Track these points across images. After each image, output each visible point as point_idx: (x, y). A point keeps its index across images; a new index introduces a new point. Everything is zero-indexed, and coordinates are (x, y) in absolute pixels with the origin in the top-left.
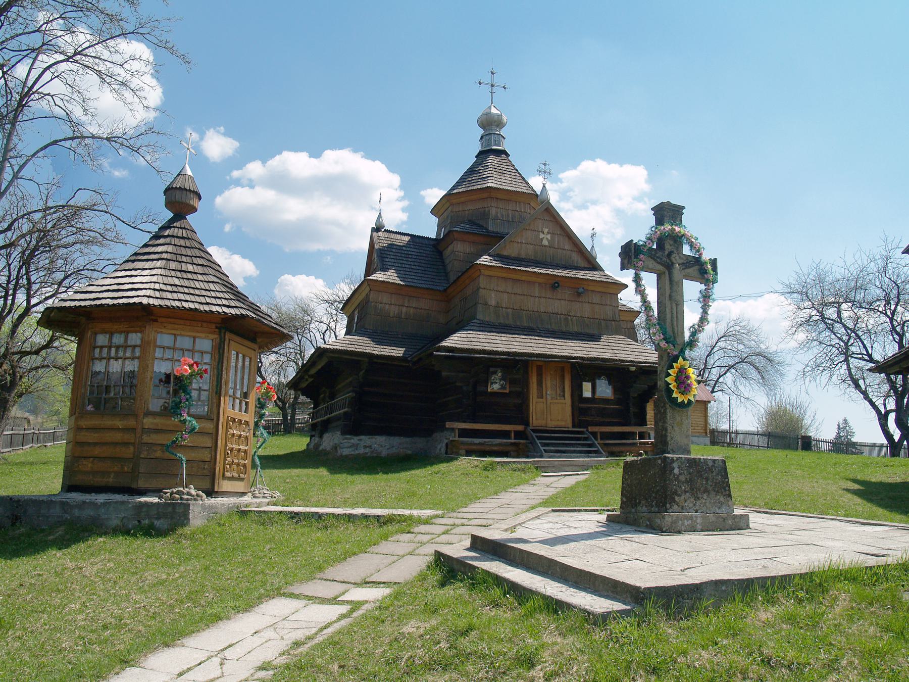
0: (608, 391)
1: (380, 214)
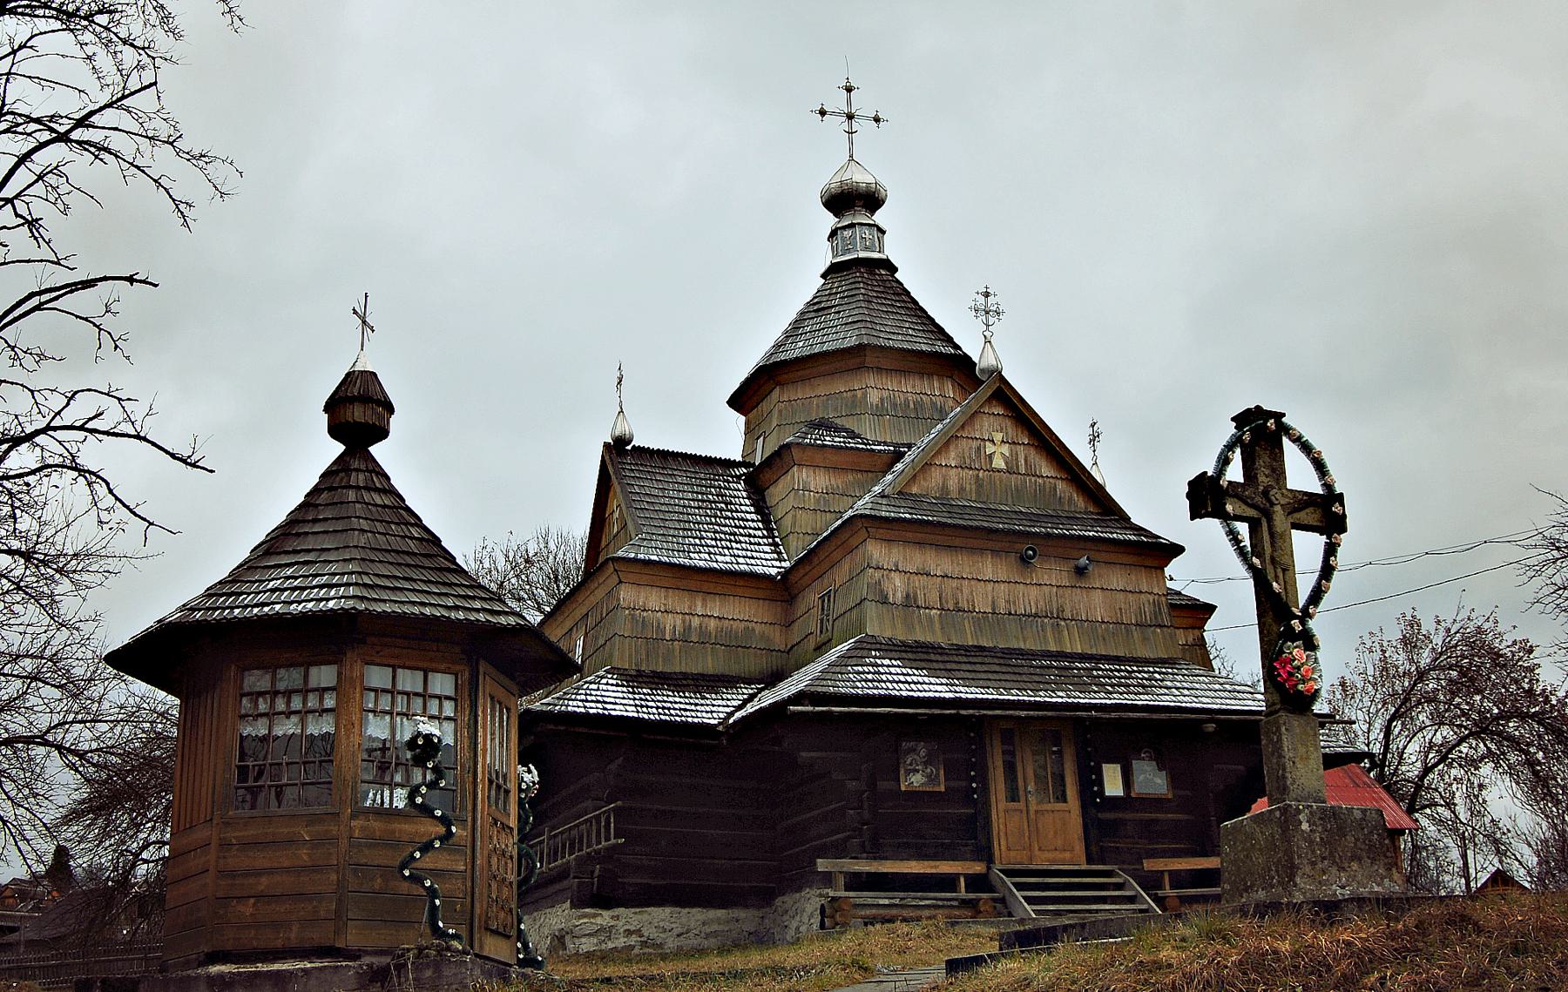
0: (1159, 781)
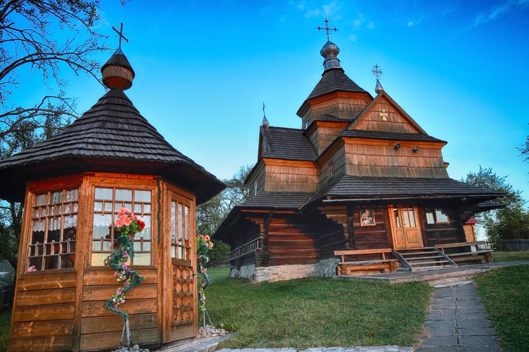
1: (265, 117)
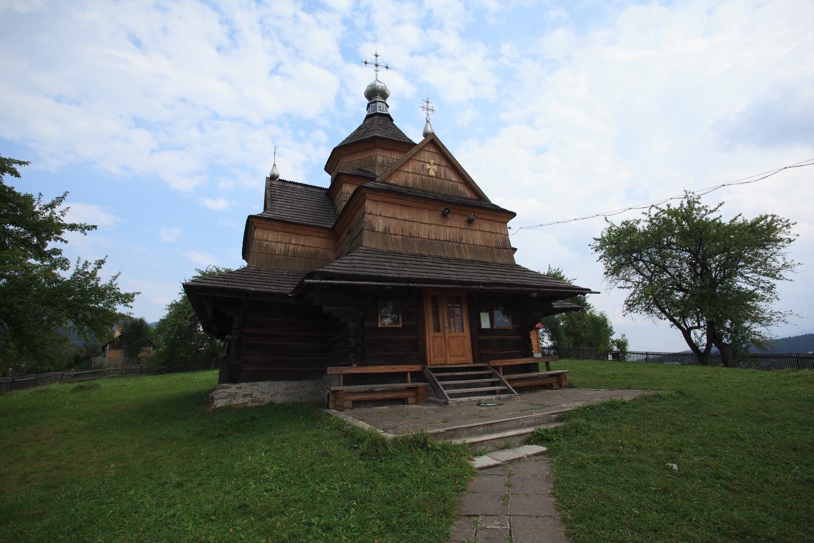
0: (506, 321)
1: (274, 165)
